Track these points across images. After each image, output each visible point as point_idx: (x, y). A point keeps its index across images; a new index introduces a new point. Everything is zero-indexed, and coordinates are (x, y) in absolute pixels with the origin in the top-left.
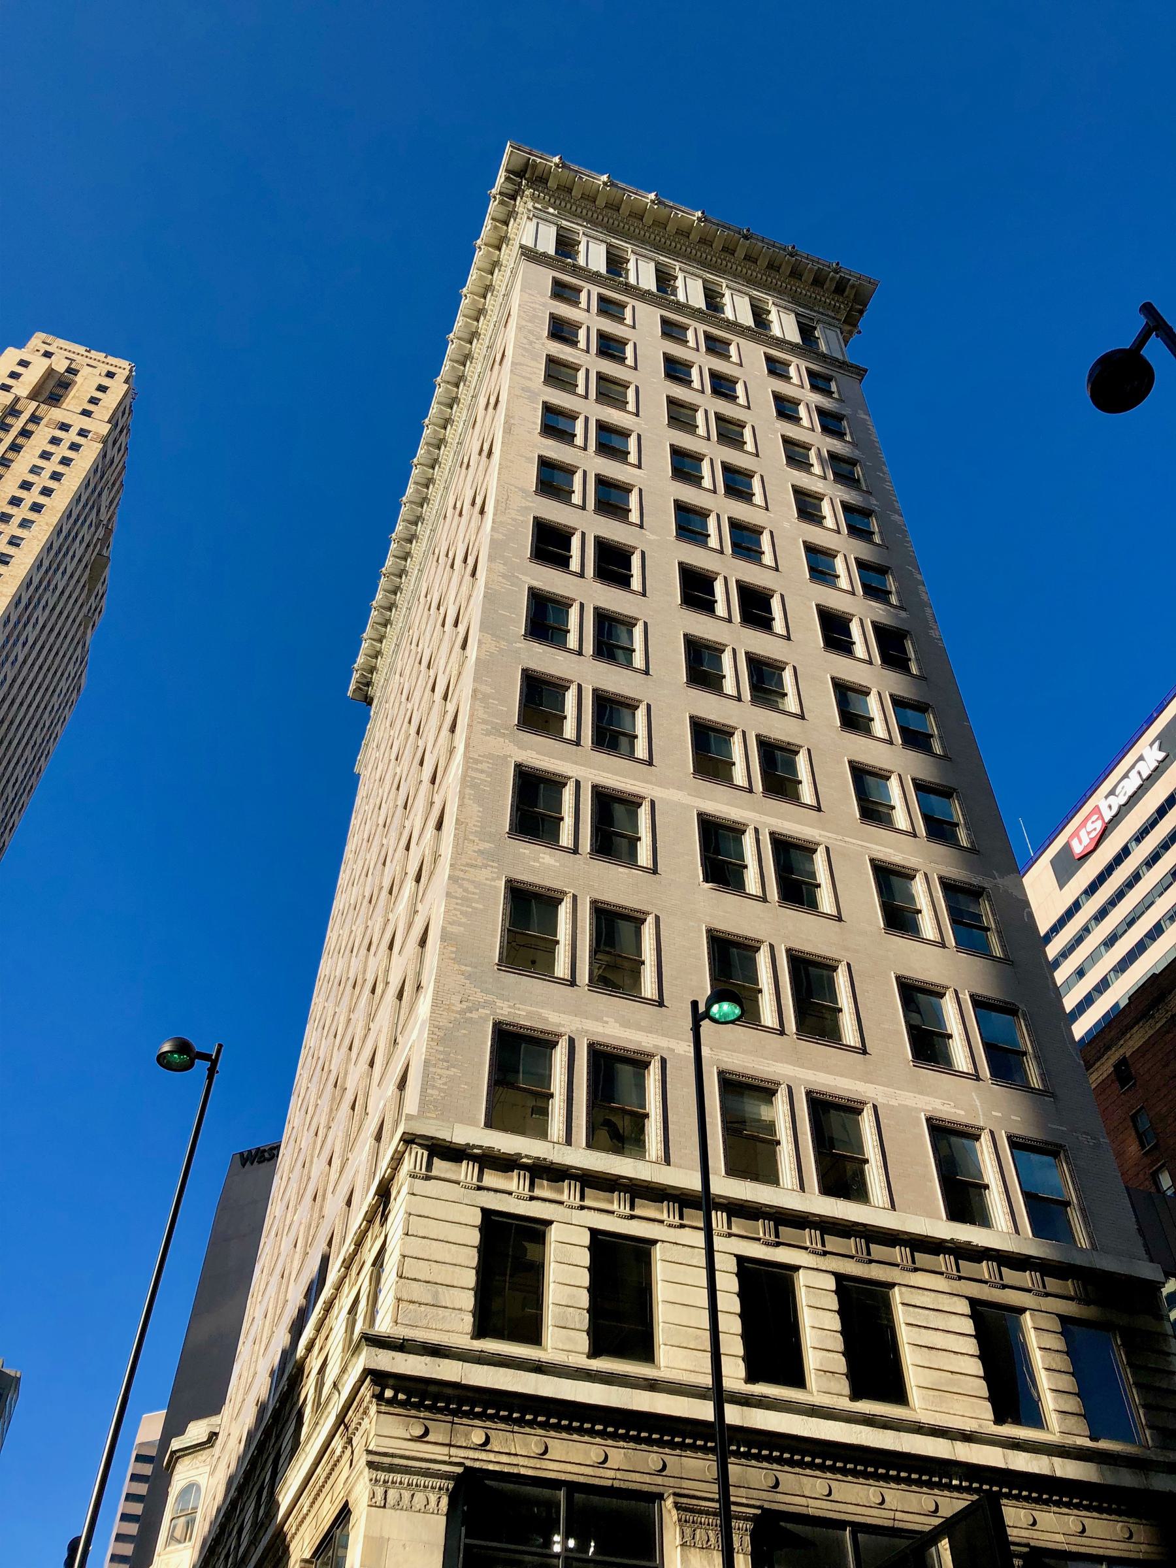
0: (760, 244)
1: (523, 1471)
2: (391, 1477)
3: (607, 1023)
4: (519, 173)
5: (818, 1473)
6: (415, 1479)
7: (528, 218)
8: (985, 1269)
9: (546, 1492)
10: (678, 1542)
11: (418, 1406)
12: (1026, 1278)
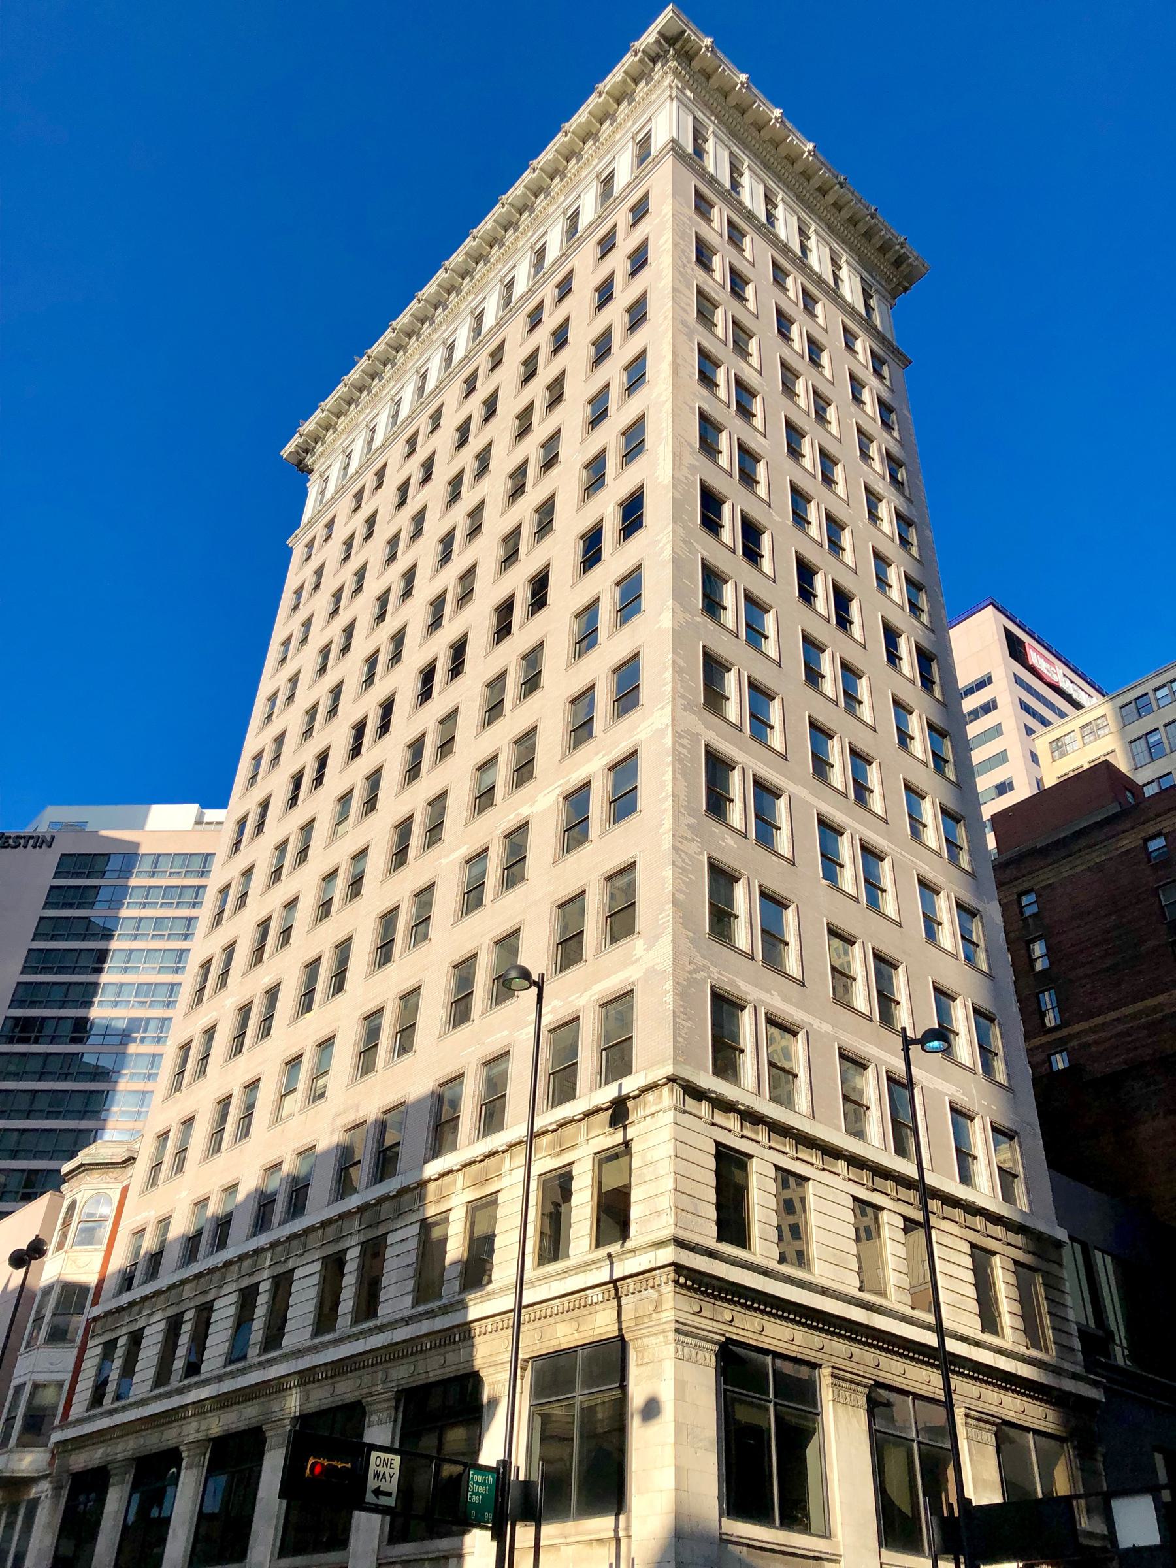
0: (850, 195)
1: (752, 1342)
3: (773, 995)
4: (670, 39)
5: (899, 1358)
6: (699, 1342)
7: (670, 96)
10: (831, 1398)
11: (696, 1291)
12: (999, 1231)
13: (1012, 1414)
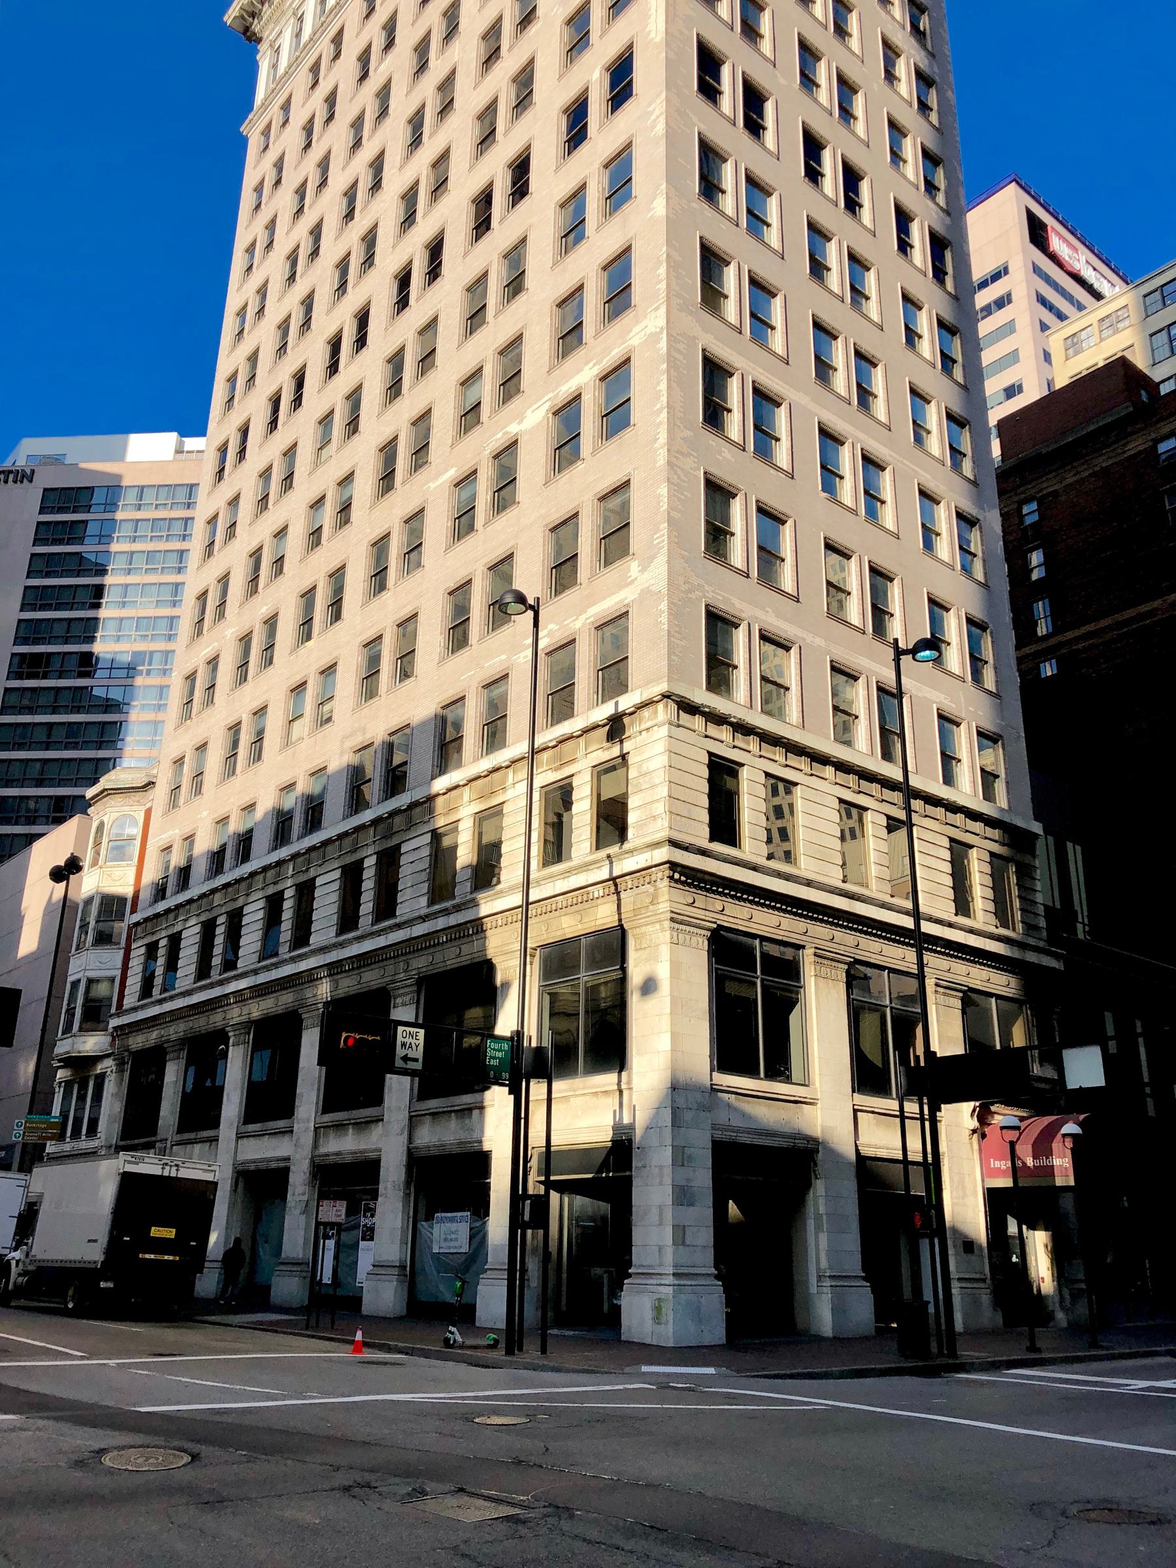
1: (741, 928)
2: (681, 927)
3: (767, 612)
8: (959, 819)
9: (749, 940)
10: (813, 973)
12: (978, 827)
13: (978, 982)
